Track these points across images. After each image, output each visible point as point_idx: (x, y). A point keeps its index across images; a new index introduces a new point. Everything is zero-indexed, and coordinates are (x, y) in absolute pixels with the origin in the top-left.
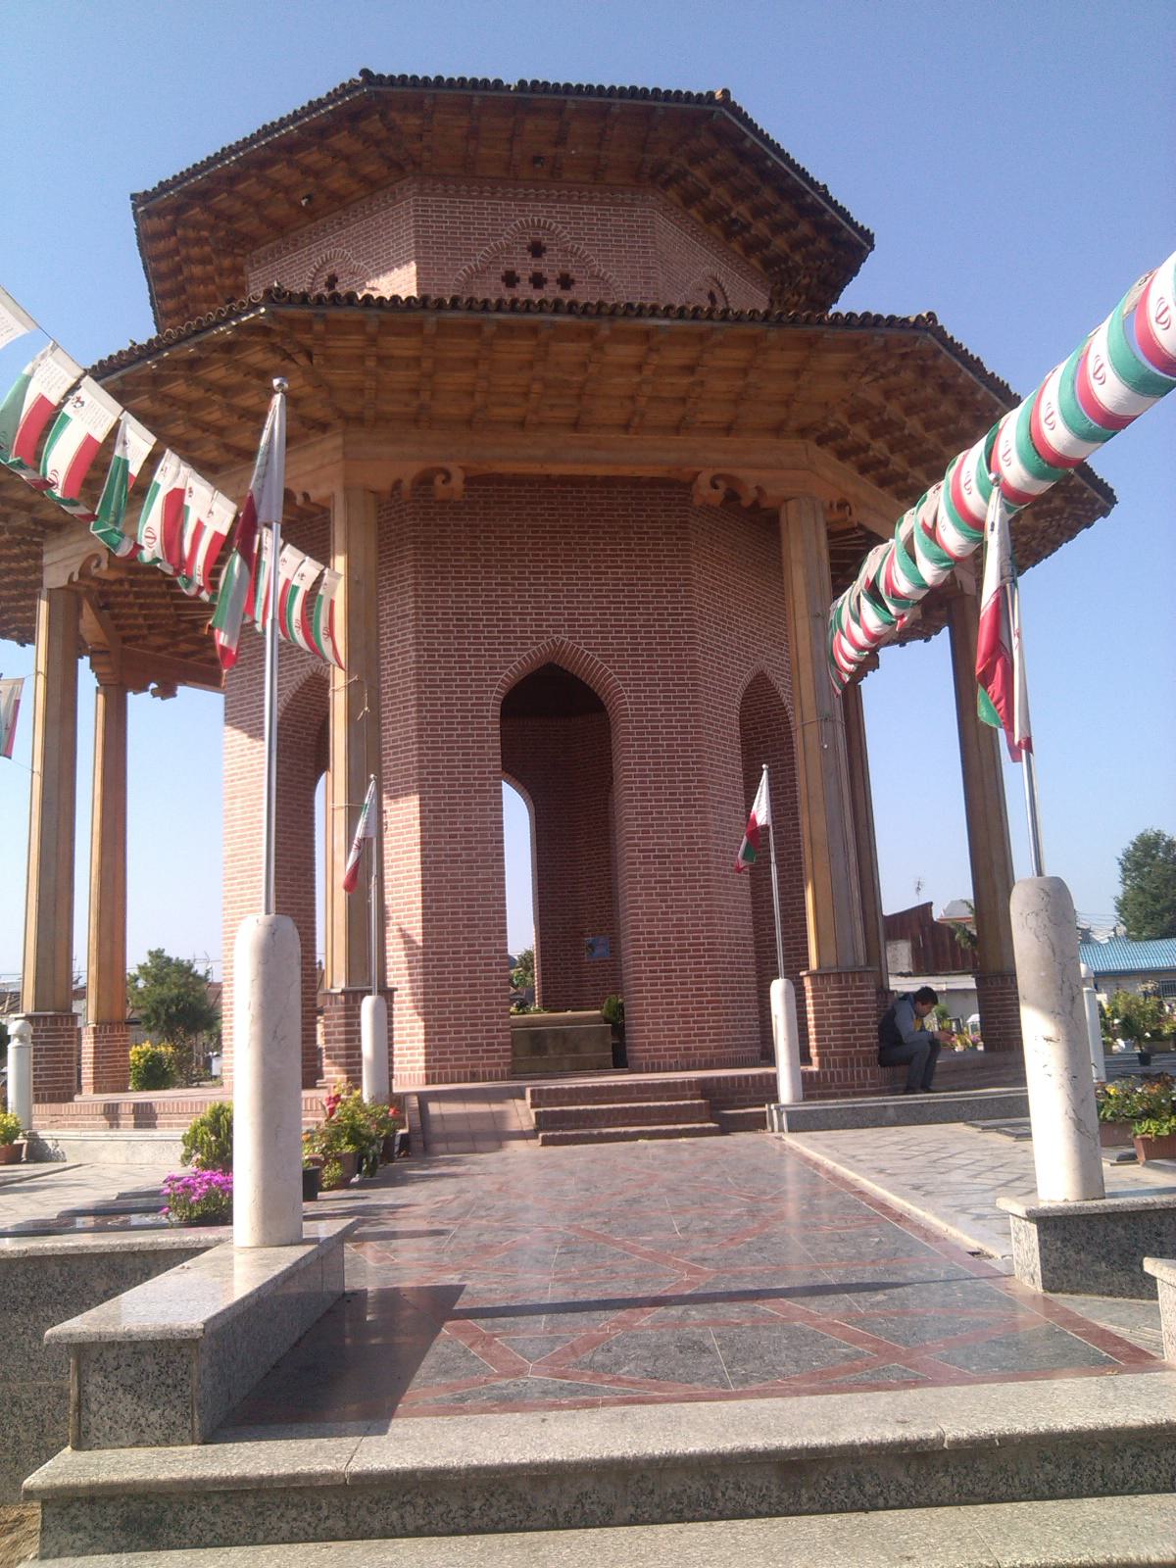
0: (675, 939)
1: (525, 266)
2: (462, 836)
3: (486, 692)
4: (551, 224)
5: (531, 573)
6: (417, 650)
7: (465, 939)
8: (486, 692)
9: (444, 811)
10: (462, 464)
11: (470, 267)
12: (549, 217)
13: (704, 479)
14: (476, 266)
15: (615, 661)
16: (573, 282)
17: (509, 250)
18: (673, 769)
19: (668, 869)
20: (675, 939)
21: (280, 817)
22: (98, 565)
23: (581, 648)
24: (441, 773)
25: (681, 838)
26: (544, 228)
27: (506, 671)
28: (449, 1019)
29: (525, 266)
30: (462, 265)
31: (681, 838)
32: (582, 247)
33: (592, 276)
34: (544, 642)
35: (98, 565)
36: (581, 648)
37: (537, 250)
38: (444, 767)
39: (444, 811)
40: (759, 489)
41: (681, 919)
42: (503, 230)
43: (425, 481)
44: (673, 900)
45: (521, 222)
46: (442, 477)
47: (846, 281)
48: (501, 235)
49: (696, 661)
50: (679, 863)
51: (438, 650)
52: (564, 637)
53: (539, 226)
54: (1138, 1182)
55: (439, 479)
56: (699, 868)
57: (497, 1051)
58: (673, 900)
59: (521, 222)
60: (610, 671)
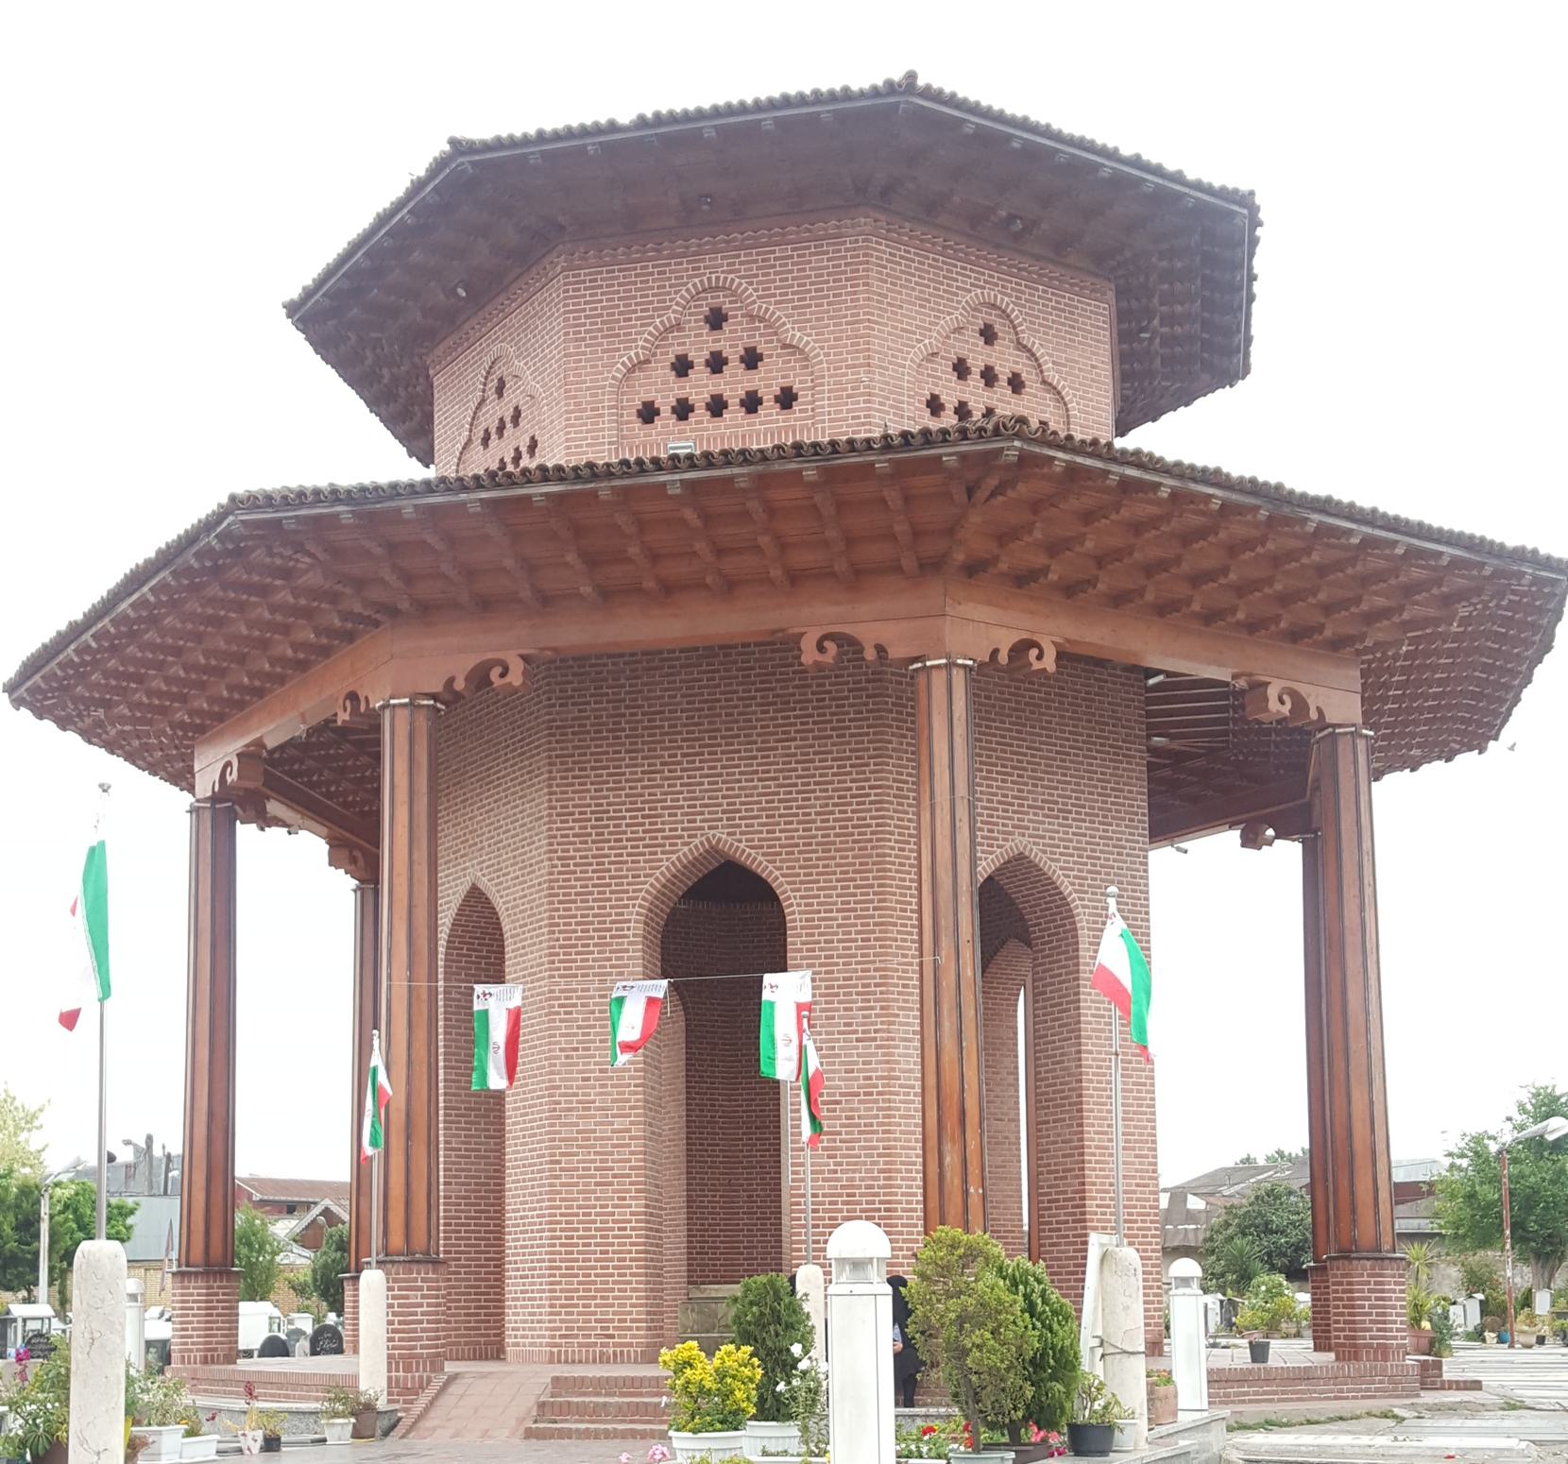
0: (844, 1203)
1: (699, 345)
2: (596, 1079)
3: (627, 906)
5: (684, 755)
6: (550, 859)
7: (597, 1199)
8: (627, 906)
9: (576, 1049)
10: (525, 652)
15: (782, 861)
16: (760, 358)
18: (850, 994)
19: (839, 1118)
20: (844, 1203)
21: (1007, 1061)
23: (742, 845)
24: (575, 1005)
25: (857, 1079)
26: (724, 288)
27: (652, 880)
28: (577, 1290)
29: (699, 345)
31: (857, 1079)
33: (785, 346)
34: (697, 841)
36: (742, 845)
37: (716, 320)
39: (576, 1049)
40: (880, 649)
41: (853, 1179)
43: (480, 678)
44: (843, 1156)
49: (884, 855)
50: (852, 1110)
51: (573, 858)
52: (722, 834)
54: (4, 1182)
55: (495, 674)
56: (877, 1117)
57: (630, 1329)
58: (843, 1156)
60: (777, 873)
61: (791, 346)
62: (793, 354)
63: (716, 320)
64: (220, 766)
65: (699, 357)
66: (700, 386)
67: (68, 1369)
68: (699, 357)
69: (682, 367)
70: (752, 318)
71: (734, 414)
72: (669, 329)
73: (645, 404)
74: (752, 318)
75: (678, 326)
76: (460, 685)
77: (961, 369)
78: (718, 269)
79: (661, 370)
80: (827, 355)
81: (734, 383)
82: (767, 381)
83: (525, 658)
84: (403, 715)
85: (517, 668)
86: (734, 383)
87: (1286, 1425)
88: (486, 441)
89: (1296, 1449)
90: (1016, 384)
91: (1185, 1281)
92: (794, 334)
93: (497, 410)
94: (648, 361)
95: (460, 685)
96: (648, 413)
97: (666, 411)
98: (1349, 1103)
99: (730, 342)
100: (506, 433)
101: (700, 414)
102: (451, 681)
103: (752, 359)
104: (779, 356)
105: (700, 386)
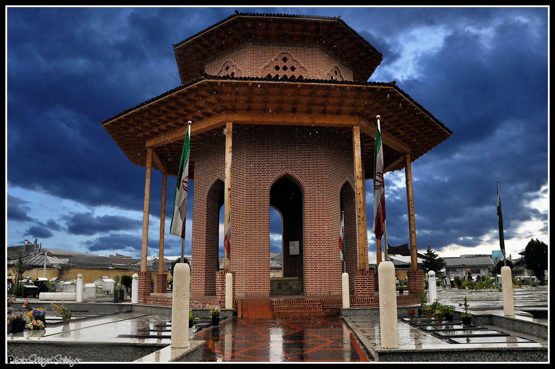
1: (281, 64)
29: (281, 64)
37: (285, 60)
63: (285, 60)
65: (281, 67)
66: (281, 73)
67: (58, 292)
68: (281, 67)
70: (293, 60)
74: (293, 60)
78: (286, 50)
79: (272, 68)
81: (289, 74)
87: (525, 333)
89: (131, 236)
91: (432, 276)
92: (302, 65)
98: (480, 256)
99: (289, 64)
103: (293, 69)
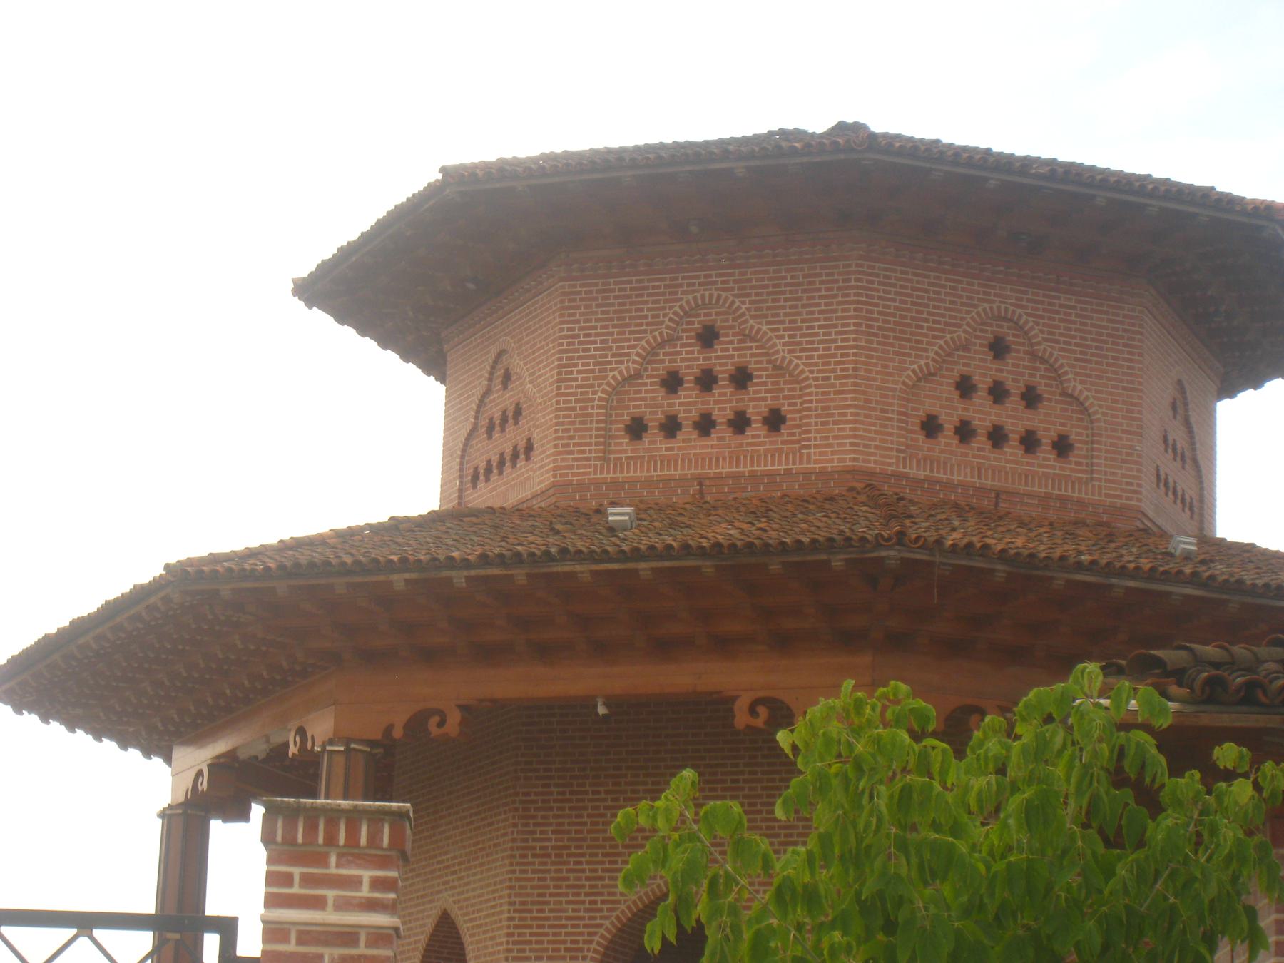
1: (984, 371)
4: (1020, 316)
11: (920, 367)
12: (1018, 306)
13: (741, 706)
14: (927, 365)
17: (670, 340)
22: (441, 724)
26: (1011, 320)
30: (912, 363)
32: (1056, 353)
33: (1064, 394)
35: (441, 724)
37: (998, 349)
38: (585, 926)
42: (962, 319)
43: (417, 723)
45: (984, 310)
46: (436, 719)
47: (407, 520)
48: (960, 326)
53: (697, 306)
59: (984, 310)
61: (1071, 396)
62: (1070, 404)
63: (708, 337)
64: (192, 773)
69: (672, 383)
71: (1012, 450)
72: (662, 344)
73: (633, 419)
74: (1033, 355)
75: (670, 340)
76: (398, 733)
77: (965, 387)
79: (946, 388)
80: (1105, 414)
81: (1014, 418)
82: (1047, 422)
83: (464, 708)
84: (341, 760)
85: (454, 718)
86: (722, 403)
88: (490, 430)
90: (1031, 398)
93: (502, 401)
94: (934, 375)
95: (398, 733)
96: (637, 429)
97: (949, 429)
100: (512, 408)
101: (981, 440)
102: (389, 728)
103: (742, 378)
104: (1057, 402)
105: (688, 403)
